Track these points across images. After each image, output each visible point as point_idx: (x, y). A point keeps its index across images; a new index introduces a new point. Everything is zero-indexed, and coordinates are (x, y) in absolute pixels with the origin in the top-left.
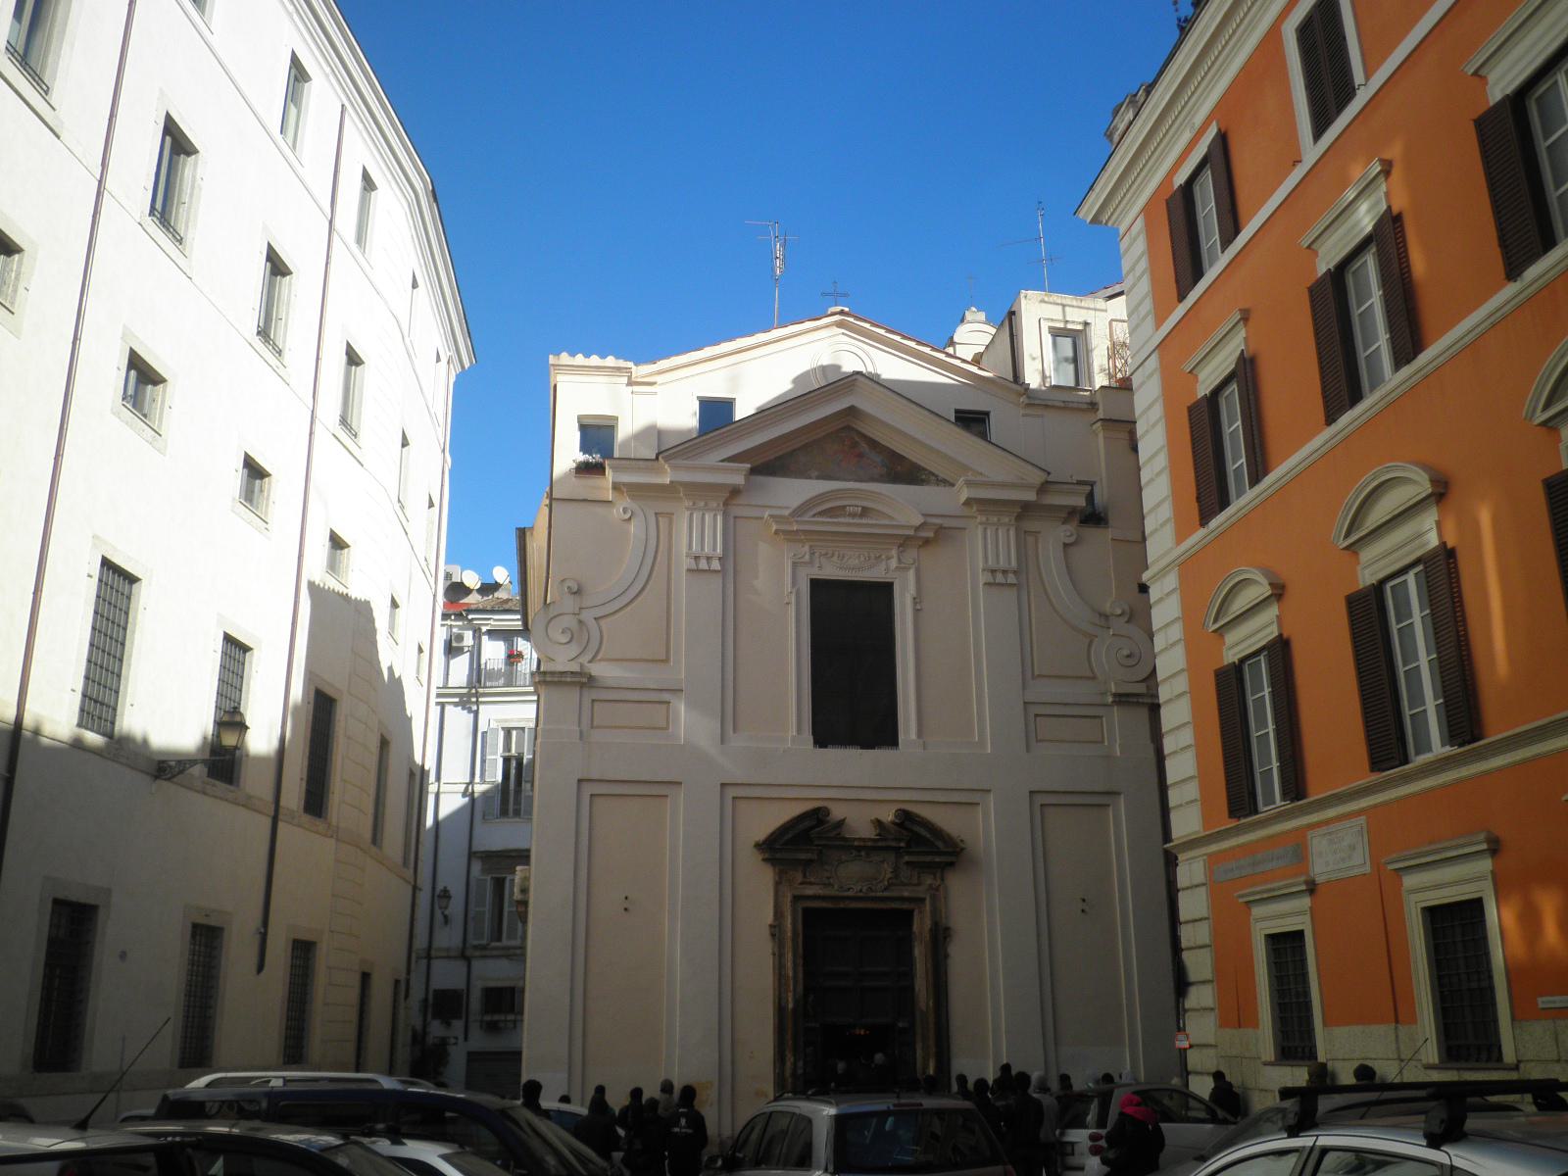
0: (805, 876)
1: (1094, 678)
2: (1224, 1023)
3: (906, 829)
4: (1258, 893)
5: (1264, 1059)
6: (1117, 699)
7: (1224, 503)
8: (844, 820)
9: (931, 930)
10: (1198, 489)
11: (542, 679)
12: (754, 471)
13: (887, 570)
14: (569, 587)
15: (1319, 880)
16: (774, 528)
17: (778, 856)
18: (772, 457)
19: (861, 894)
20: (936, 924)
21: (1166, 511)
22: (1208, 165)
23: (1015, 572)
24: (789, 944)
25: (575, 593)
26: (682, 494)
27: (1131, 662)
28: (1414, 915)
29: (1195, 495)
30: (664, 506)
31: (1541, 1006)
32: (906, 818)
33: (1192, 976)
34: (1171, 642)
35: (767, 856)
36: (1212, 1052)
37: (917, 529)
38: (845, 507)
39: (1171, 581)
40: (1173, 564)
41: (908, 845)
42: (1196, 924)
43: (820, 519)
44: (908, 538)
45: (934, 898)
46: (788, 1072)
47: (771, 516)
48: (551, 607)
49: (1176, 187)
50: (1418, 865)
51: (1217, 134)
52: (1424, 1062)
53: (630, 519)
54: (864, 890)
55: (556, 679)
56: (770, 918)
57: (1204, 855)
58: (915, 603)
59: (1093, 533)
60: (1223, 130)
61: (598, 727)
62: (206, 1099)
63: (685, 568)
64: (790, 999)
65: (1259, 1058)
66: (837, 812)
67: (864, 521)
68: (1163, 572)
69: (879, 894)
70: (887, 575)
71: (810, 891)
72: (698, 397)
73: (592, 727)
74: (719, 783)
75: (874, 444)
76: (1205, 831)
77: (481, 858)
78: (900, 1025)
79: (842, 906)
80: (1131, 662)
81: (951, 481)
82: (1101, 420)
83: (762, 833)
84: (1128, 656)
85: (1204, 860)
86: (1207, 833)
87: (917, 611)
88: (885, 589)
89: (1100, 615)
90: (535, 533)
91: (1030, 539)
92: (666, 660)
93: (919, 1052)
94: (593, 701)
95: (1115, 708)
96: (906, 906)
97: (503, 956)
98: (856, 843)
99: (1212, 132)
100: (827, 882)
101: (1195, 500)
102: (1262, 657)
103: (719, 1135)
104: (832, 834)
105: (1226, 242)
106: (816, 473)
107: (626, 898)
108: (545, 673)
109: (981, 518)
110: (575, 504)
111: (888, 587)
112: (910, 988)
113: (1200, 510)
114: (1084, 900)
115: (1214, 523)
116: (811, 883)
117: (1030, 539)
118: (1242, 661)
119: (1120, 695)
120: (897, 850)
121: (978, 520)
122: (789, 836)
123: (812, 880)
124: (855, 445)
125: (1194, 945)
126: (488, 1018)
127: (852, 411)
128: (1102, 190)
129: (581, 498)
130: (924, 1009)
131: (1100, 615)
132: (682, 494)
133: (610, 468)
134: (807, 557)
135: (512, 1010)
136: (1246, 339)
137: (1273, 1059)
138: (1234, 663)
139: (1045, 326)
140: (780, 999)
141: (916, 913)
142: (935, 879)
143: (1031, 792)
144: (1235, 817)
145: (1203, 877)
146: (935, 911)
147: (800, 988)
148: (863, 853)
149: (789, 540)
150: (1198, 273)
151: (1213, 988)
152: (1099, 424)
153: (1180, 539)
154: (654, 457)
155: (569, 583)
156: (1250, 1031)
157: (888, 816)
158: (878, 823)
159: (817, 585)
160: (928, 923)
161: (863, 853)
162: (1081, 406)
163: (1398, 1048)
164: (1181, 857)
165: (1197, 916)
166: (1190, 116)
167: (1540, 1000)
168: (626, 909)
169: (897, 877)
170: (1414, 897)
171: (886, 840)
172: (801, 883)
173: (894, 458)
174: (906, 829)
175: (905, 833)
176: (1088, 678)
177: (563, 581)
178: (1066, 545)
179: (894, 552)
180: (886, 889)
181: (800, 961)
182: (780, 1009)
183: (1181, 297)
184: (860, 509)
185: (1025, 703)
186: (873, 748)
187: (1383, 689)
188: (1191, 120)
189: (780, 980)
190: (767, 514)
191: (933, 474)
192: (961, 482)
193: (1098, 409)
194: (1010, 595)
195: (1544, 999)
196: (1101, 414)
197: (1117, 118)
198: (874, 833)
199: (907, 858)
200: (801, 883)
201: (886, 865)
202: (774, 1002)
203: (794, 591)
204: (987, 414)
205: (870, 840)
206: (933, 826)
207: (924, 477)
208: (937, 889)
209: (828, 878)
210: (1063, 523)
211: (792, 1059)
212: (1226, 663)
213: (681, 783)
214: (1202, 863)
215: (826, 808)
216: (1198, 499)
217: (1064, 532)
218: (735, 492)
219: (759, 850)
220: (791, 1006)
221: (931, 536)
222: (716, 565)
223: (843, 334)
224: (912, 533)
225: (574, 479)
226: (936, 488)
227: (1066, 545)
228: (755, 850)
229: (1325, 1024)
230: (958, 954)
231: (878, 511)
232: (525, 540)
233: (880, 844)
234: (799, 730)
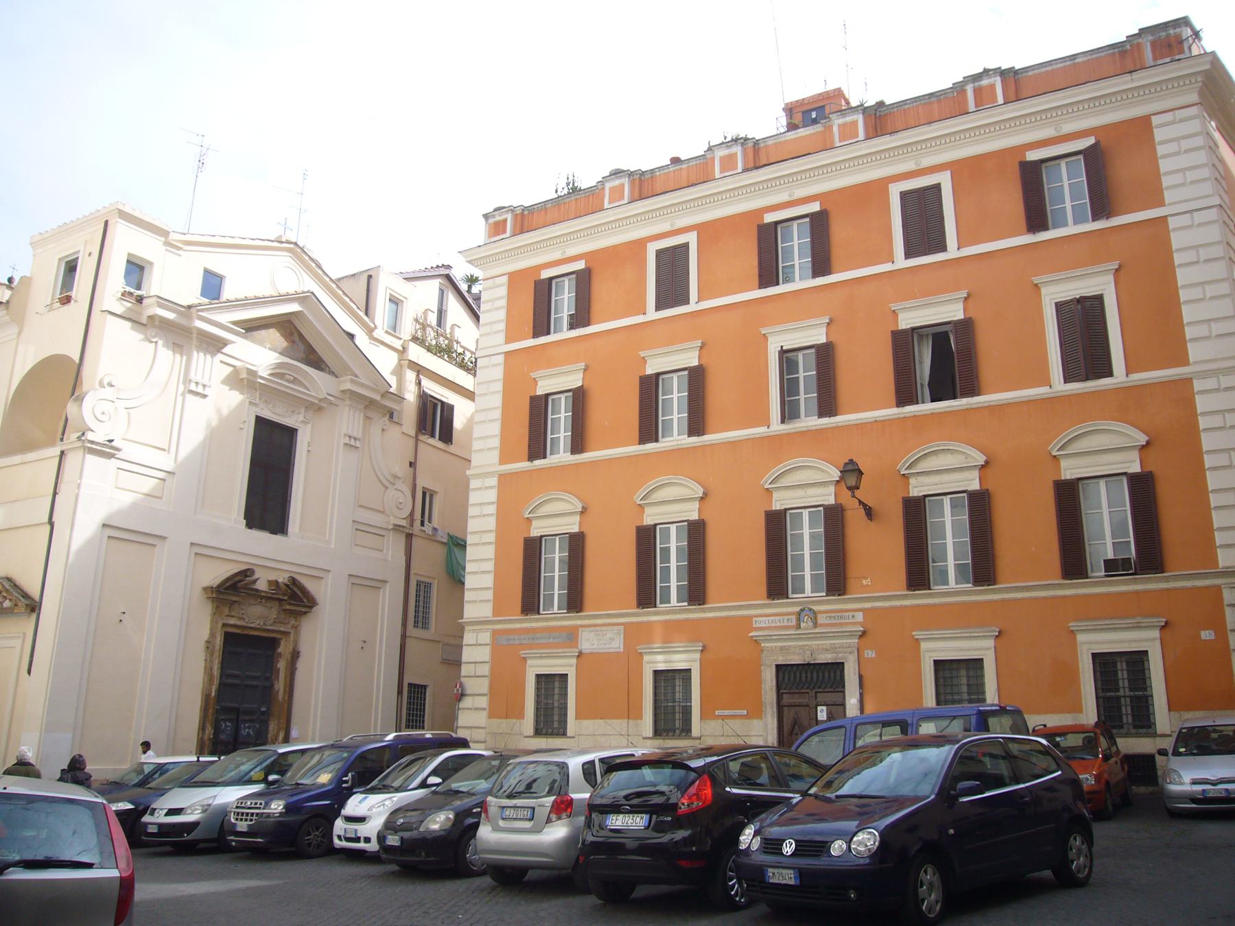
2: (492, 715)
6: (395, 527)
15: (583, 651)
17: (221, 596)
19: (259, 627)
20: (294, 649)
28: (648, 673)
31: (717, 714)
32: (294, 581)
37: (320, 400)
38: (285, 374)
44: (312, 404)
50: (649, 652)
52: (644, 736)
62: (282, 745)
71: (232, 621)
74: (189, 542)
95: (392, 532)
96: (278, 636)
98: (263, 594)
100: (241, 616)
116: (233, 616)
120: (280, 600)
122: (229, 584)
137: (651, 736)
139: (389, 291)
148: (263, 601)
157: (282, 578)
163: (628, 731)
164: (467, 628)
167: (717, 712)
170: (648, 666)
172: (228, 616)
175: (289, 591)
186: (276, 534)
191: (328, 367)
195: (719, 711)
207: (323, 367)
209: (243, 614)
213: (165, 538)
221: (316, 408)
223: (291, 257)
224: (316, 402)
226: (327, 375)
229: (578, 717)
230: (301, 665)
231: (299, 381)
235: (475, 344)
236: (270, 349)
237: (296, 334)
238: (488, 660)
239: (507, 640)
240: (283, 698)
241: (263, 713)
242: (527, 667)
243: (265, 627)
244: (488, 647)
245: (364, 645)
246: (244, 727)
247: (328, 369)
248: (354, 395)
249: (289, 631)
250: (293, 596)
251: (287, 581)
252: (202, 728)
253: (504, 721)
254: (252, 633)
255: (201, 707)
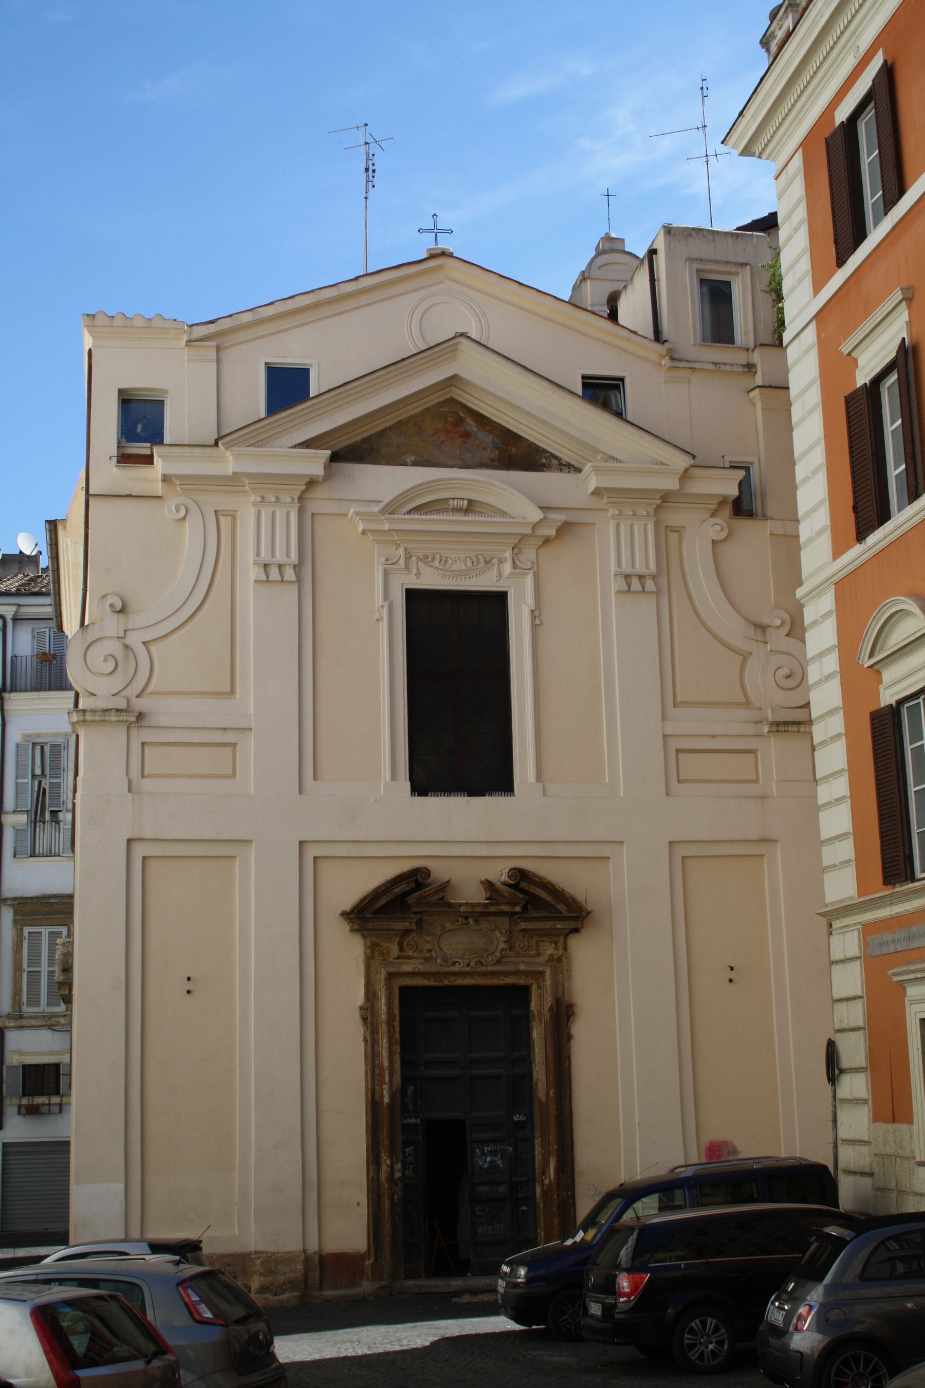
0: (401, 949)
1: (747, 703)
2: (877, 1117)
3: (522, 891)
4: (913, 972)
5: (918, 1159)
7: (884, 516)
8: (448, 882)
9: (551, 1009)
10: (855, 497)
11: (81, 718)
12: (336, 458)
13: (500, 576)
14: (111, 605)
16: (361, 527)
17: (370, 926)
18: (358, 438)
19: (468, 969)
20: (558, 1001)
21: (822, 518)
22: (872, 104)
23: (654, 577)
24: (383, 1029)
25: (119, 612)
26: (247, 488)
27: (792, 683)
28: (913, 1022)
29: (852, 504)
30: (225, 502)
32: (521, 877)
33: (845, 1063)
34: (826, 673)
35: (355, 927)
36: (865, 1150)
37: (535, 526)
38: (447, 500)
39: (827, 602)
40: (829, 582)
41: (525, 908)
42: (850, 1003)
43: (417, 517)
45: (555, 972)
46: (383, 1176)
47: (357, 513)
48: (90, 629)
49: (837, 123)
51: (883, 66)
53: (184, 518)
54: (472, 964)
55: (98, 718)
56: (360, 999)
57: (859, 923)
58: (533, 617)
59: (745, 525)
60: (889, 63)
61: (150, 776)
63: (252, 579)
64: (385, 1092)
65: (914, 1158)
66: (440, 872)
67: (470, 518)
68: (817, 591)
69: (489, 968)
70: (499, 584)
71: (407, 968)
72: (266, 364)
73: (143, 776)
75: (482, 420)
76: (860, 896)
77: (12, 905)
78: (516, 1118)
79: (446, 982)
80: (792, 683)
81: (577, 465)
82: (759, 387)
83: (349, 901)
84: (788, 677)
85: (859, 929)
86: (862, 899)
87: (535, 627)
88: (499, 599)
89: (756, 626)
90: (68, 526)
91: (673, 537)
92: (233, 691)
93: (538, 1150)
94: (143, 744)
96: (522, 981)
97: (43, 1026)
99: (877, 62)
101: (851, 507)
102: (921, 700)
103: (304, 1251)
104: (433, 899)
105: (889, 203)
106: (413, 458)
107: (189, 979)
108: (84, 711)
109: (612, 511)
110: (119, 501)
111: (501, 598)
112: (528, 1076)
113: (857, 523)
114: (732, 969)
115: (872, 539)
116: (410, 958)
117: (673, 537)
118: (900, 703)
119: (778, 724)
120: (512, 914)
121: (610, 512)
122: (383, 902)
123: (411, 953)
124: (460, 421)
125: (846, 1027)
126: (25, 1101)
127: (453, 380)
128: (753, 117)
129: (125, 494)
130: (543, 1099)
131: (756, 626)
132: (247, 488)
133: (159, 456)
134: (402, 561)
135: (57, 1092)
136: (909, 324)
138: (891, 705)
140: (373, 1092)
141: (534, 988)
142: (556, 948)
143: (670, 843)
144: (890, 884)
145: (857, 949)
146: (556, 984)
147: (398, 1077)
149: (378, 542)
150: (860, 235)
151: (867, 1077)
152: (757, 391)
153: (837, 554)
154: (212, 443)
155: (110, 600)
156: (904, 1127)
157: (499, 873)
158: (488, 885)
159: (412, 595)
160: (549, 1000)
161: (471, 921)
162: (735, 368)
165: (850, 993)
166: (854, 38)
168: (189, 992)
169: (511, 948)
171: (498, 904)
172: (398, 957)
173: (508, 437)
174: (522, 891)
175: (521, 896)
176: (737, 705)
177: (103, 597)
178: (714, 542)
179: (508, 555)
180: (498, 962)
181: (397, 1049)
182: (373, 1104)
183: (841, 262)
184: (466, 503)
185: (664, 736)
186: (484, 795)
187: (898, 869)
188: (855, 41)
189: (373, 1071)
190: (352, 511)
191: (556, 457)
192: (587, 468)
193: (756, 373)
194: (649, 604)
196: (759, 380)
197: (775, 23)
198: (484, 896)
199: (523, 925)
200: (398, 957)
201: (498, 934)
202: (367, 1095)
203: (387, 604)
204: (622, 380)
205: (479, 904)
206: (553, 886)
207: (544, 460)
208: (559, 960)
210: (712, 516)
211: (388, 1162)
212: (882, 705)
214: (856, 932)
215: (426, 869)
216: (855, 509)
217: (714, 528)
218: (311, 483)
219: (346, 919)
220: (386, 1100)
222: (290, 574)
224: (528, 531)
225: (115, 469)
227: (714, 542)
228: (341, 918)
232: (56, 534)
233: (492, 909)
234: (394, 777)
235: (326, 390)
236: (415, 464)
237: (469, 420)
238: (859, 993)
239: (881, 944)
240: (547, 1095)
241: (520, 1125)
242: (907, 1004)
243: (480, 969)
244: (858, 962)
245: (732, 975)
246: (483, 1153)
247: (554, 462)
248: (618, 495)
249: (541, 969)
250: (533, 902)
251: (507, 878)
252: (373, 1159)
253: (890, 1127)
254: (460, 981)
255: (367, 1122)
